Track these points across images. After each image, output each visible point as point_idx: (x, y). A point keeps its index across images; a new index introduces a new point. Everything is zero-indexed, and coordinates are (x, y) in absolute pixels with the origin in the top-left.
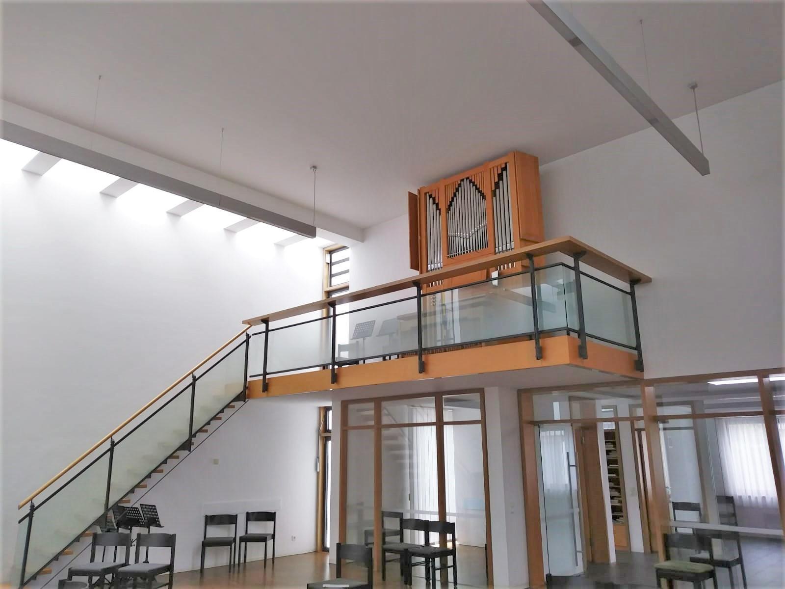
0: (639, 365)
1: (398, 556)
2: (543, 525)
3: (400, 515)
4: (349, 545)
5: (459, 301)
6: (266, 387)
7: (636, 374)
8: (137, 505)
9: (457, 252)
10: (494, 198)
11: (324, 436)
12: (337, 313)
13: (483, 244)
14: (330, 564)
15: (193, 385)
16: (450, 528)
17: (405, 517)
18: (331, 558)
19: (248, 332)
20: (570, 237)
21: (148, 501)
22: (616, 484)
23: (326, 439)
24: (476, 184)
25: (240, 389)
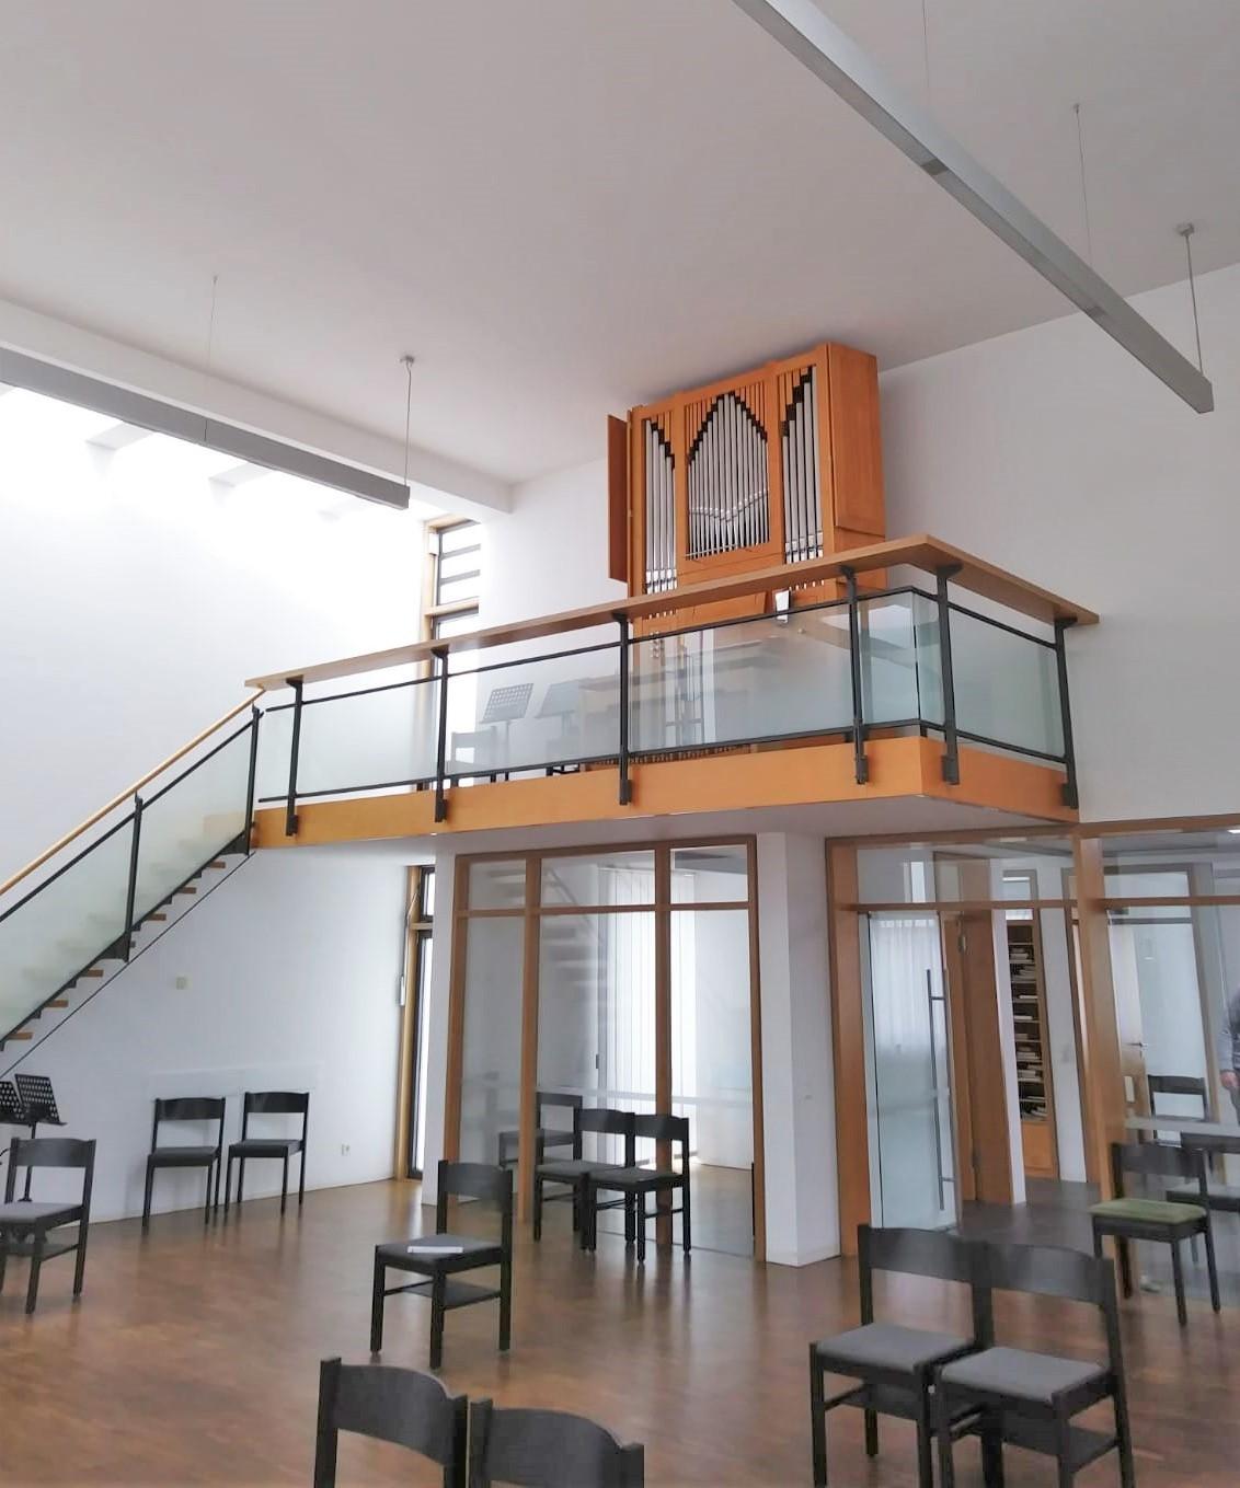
0: (1068, 794)
1: (569, 1189)
2: (872, 1122)
3: (575, 1102)
4: (464, 1164)
5: (715, 651)
6: (294, 824)
7: (1064, 814)
8: (10, 1078)
9: (708, 550)
10: (785, 439)
11: (418, 928)
12: (450, 672)
13: (765, 531)
14: (423, 1205)
15: (136, 817)
16: (679, 1129)
17: (585, 1106)
18: (426, 1193)
19: (257, 704)
20: (929, 537)
21: (34, 1067)
22: (1032, 1036)
23: (422, 935)
24: (748, 406)
25: (238, 826)
